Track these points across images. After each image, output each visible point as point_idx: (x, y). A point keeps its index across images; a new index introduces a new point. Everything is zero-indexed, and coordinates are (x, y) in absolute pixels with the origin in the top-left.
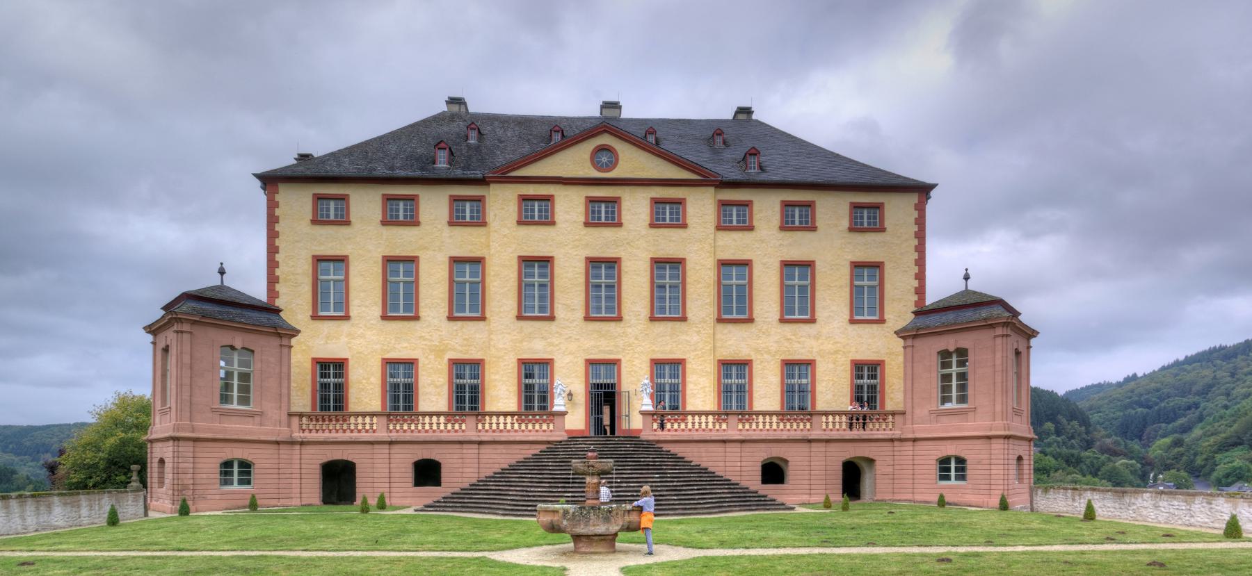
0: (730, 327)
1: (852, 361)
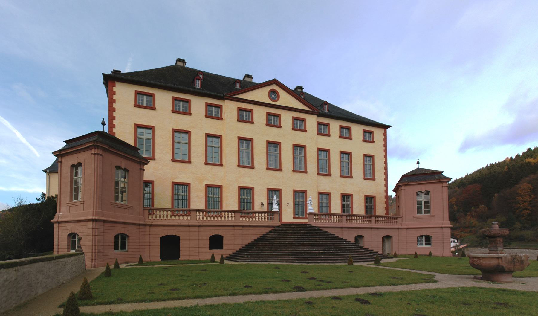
0: (322, 177)
1: (341, 194)
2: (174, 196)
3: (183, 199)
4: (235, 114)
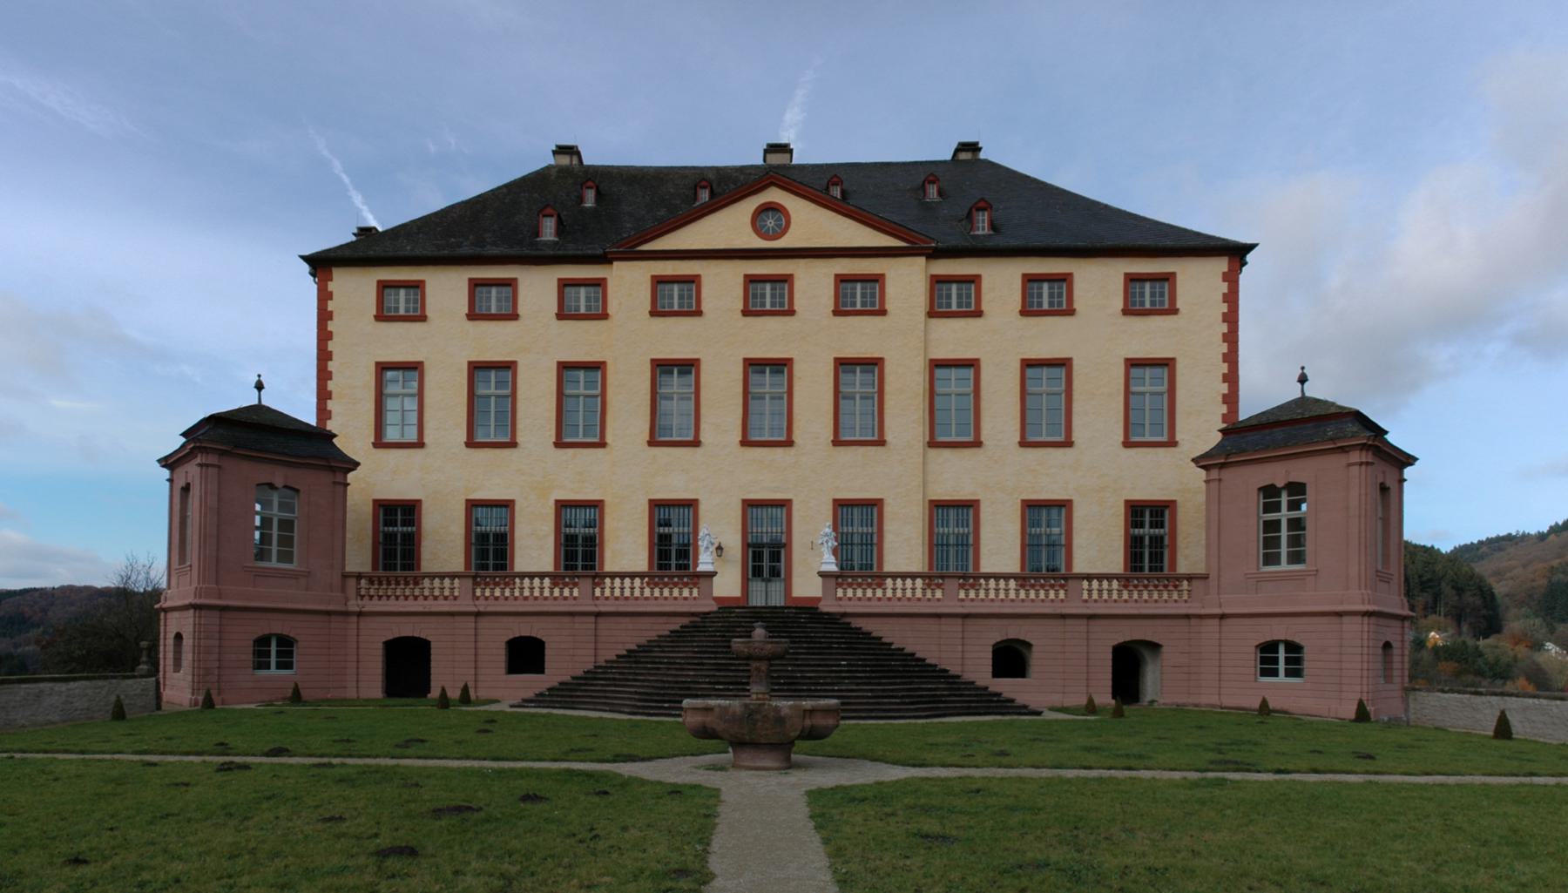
0: (947, 453)
1: (1127, 502)
2: (935, 537)
3: (847, 540)
4: (643, 296)
